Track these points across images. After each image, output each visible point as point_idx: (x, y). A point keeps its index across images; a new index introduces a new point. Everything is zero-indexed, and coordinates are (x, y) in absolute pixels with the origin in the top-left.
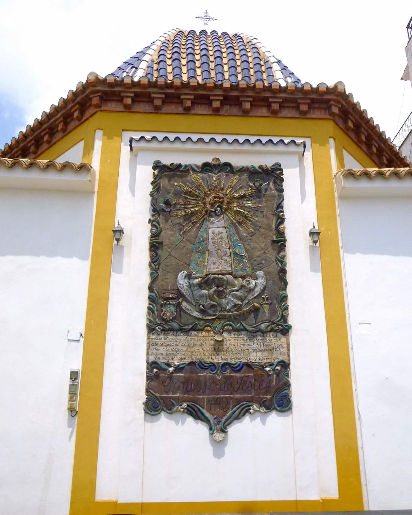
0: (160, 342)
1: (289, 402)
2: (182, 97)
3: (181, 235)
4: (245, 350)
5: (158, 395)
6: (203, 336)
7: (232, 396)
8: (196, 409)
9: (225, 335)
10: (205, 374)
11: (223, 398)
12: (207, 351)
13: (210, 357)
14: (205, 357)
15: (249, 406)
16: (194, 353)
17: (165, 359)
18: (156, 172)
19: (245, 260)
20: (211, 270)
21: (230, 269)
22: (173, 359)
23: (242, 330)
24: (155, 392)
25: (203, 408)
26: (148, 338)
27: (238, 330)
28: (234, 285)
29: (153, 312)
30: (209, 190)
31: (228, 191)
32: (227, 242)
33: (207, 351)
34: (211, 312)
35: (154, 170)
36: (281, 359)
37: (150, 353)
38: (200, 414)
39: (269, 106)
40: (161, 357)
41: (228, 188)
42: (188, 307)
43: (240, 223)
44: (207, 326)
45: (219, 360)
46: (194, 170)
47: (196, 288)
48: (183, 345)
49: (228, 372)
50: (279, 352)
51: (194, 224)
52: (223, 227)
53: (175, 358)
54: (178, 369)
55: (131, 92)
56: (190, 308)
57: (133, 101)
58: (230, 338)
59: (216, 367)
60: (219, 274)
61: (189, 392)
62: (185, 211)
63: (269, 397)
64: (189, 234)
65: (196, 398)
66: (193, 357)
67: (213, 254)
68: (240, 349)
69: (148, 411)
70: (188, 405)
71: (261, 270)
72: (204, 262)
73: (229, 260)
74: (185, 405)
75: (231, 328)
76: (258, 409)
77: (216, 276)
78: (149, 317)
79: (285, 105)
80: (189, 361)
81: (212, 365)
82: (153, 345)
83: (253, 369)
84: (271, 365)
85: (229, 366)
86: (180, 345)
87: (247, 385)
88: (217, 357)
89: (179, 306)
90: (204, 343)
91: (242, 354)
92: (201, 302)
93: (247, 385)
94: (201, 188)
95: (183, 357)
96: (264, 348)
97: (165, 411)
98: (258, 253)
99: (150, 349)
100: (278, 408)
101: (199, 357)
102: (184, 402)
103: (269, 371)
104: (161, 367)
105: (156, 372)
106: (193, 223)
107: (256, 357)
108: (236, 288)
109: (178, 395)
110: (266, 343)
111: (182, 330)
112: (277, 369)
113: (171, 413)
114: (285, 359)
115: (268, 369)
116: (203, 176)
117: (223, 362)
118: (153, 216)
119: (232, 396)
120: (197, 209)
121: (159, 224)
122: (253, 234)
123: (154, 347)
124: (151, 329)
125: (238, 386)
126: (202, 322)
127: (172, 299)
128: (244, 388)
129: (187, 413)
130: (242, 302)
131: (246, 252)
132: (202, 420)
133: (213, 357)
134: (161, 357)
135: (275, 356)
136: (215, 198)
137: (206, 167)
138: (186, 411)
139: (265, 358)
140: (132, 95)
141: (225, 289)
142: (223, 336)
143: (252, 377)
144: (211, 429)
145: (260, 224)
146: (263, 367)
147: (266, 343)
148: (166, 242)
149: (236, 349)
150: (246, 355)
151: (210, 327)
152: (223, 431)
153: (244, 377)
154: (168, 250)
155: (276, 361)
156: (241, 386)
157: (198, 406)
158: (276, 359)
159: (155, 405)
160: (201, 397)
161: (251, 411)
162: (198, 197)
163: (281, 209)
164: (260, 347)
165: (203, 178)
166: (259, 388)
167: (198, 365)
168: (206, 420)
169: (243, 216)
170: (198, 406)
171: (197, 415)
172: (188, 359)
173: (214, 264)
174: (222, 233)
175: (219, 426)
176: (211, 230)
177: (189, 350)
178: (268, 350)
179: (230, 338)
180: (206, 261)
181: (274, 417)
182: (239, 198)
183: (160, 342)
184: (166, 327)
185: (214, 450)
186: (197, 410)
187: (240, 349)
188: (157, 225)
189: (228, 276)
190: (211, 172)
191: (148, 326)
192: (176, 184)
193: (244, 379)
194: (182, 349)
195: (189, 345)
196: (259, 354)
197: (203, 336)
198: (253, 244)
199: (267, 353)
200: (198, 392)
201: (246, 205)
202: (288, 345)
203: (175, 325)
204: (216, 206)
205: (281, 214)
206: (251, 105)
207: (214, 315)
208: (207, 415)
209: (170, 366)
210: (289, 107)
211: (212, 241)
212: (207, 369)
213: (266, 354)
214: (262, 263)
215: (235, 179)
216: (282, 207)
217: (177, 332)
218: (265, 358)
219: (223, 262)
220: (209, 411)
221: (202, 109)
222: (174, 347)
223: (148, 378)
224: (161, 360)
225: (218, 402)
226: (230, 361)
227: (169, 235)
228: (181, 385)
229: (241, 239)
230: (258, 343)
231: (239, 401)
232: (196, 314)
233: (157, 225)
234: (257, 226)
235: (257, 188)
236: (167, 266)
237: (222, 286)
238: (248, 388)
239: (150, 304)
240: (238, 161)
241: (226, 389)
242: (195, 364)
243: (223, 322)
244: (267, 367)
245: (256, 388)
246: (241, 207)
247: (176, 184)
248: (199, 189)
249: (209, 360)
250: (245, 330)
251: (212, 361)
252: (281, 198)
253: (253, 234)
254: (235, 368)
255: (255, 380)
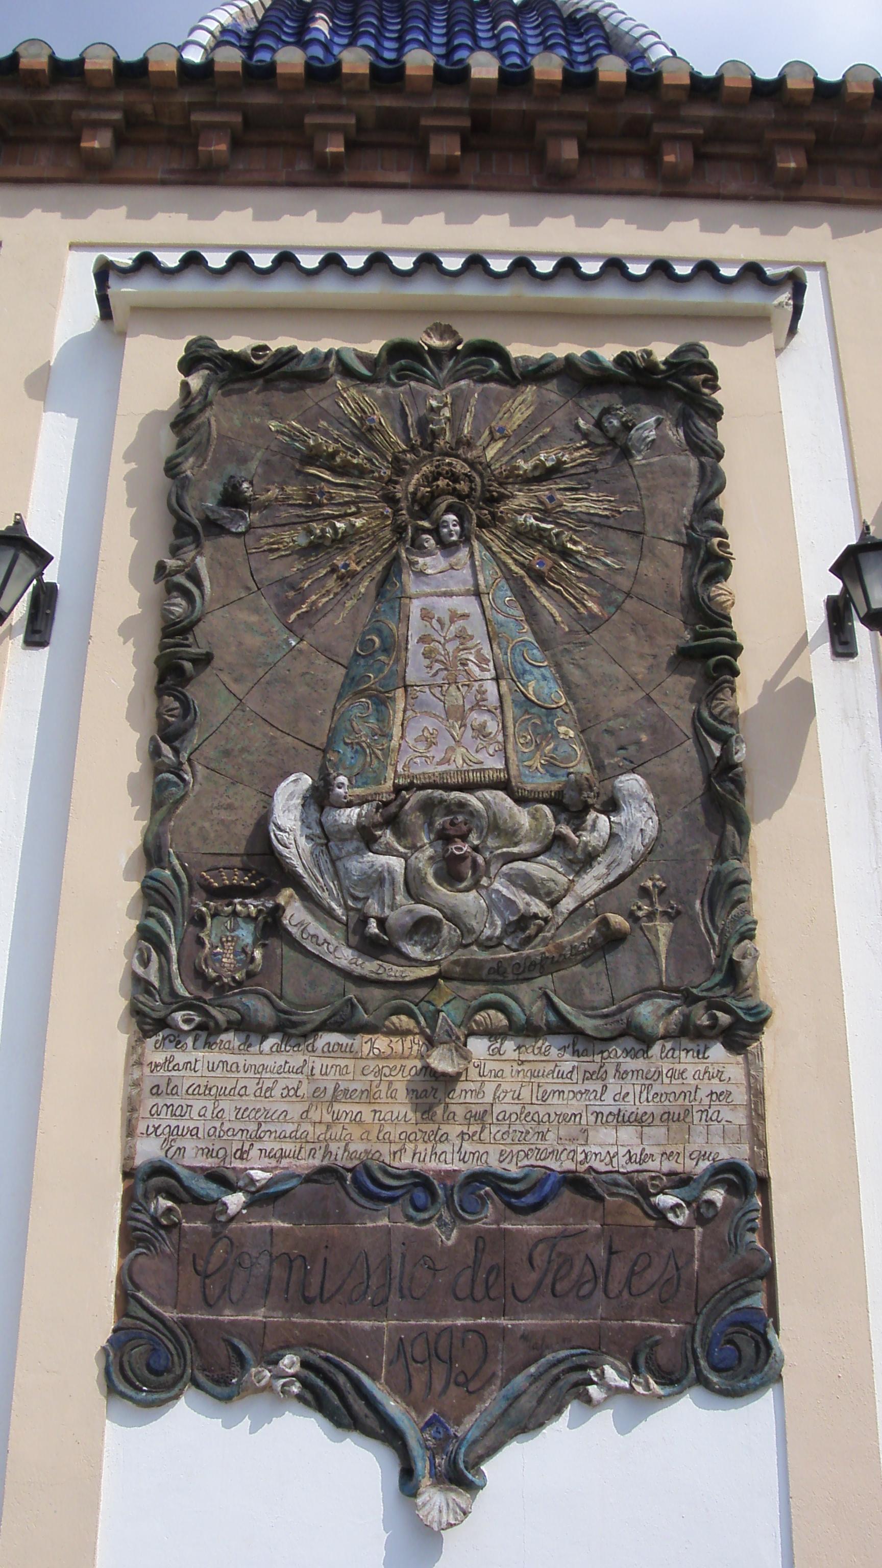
0: (186, 1079)
1: (764, 1349)
2: (309, 120)
3: (289, 628)
4: (564, 1118)
5: (170, 1314)
6: (379, 1057)
7: (503, 1322)
8: (341, 1379)
9: (478, 1046)
10: (385, 1222)
11: (467, 1329)
12: (394, 1122)
13: (410, 1147)
14: (385, 1149)
15: (583, 1368)
16: (337, 1130)
17: (209, 1153)
18: (196, 382)
19: (562, 729)
20: (414, 771)
21: (501, 766)
22: (242, 1155)
23: (552, 1031)
24: (160, 1303)
25: (374, 1377)
26: (135, 1060)
27: (527, 1030)
28: (511, 835)
29: (162, 949)
30: (413, 449)
31: (490, 453)
32: (486, 652)
33: (394, 1122)
34: (415, 951)
35: (187, 375)
36: (725, 1154)
37: (141, 1127)
38: (359, 1406)
39: (652, 158)
40: (190, 1145)
41: (493, 439)
42: (315, 927)
43: (540, 578)
44: (397, 1011)
45: (448, 1155)
46: (347, 371)
47: (351, 846)
48: (291, 1093)
49: (488, 1218)
50: (715, 1127)
51: (347, 578)
52: (467, 593)
53: (254, 1153)
54: (263, 1198)
55: (112, 108)
56: (323, 933)
57: (120, 141)
58: (496, 1066)
59: (433, 1194)
60: (449, 788)
61: (308, 1301)
62: (310, 532)
63: (673, 1327)
64: (323, 622)
65: (343, 1330)
66: (333, 1147)
67: (422, 704)
68: (542, 1111)
69: (123, 1387)
70: (305, 1364)
71: (633, 771)
72: (389, 736)
73: (493, 727)
74: (290, 1362)
75: (500, 1019)
76: (626, 1384)
77: (438, 793)
78: (140, 970)
79: (715, 149)
80: (317, 1162)
81: (421, 1181)
82: (156, 1091)
83: (600, 1199)
84: (680, 1181)
85: (498, 1190)
86: (277, 1092)
87: (574, 1275)
88: (440, 1148)
89: (271, 926)
90: (384, 1087)
91: (551, 1136)
92: (373, 907)
93: (574, 1275)
94: (378, 439)
95: (288, 1147)
96: (650, 1108)
97: (198, 1385)
98: (620, 702)
99: (144, 1112)
100: (714, 1378)
101: (358, 1147)
102: (288, 1347)
103: (674, 1208)
104: (187, 1189)
105: (164, 1208)
106: (341, 578)
107: (611, 1149)
108: (525, 848)
109: (259, 1315)
110: (657, 1088)
111: (291, 1029)
112: (711, 1203)
113: (228, 1399)
114: (741, 1153)
115: (666, 1200)
116: (386, 396)
117: (465, 1168)
118: (175, 551)
119: (503, 1322)
120: (358, 522)
121: (199, 584)
122: (594, 623)
123: (160, 1101)
124: (149, 1019)
125: (534, 1276)
126: (377, 993)
127: (245, 892)
128: (558, 1287)
129: (300, 1397)
130: (553, 905)
131: (569, 694)
132: (368, 1433)
133: (421, 1147)
134: (190, 1145)
135: (698, 1143)
136: (436, 476)
137: (403, 358)
138: (296, 1389)
139: (656, 1151)
140: (117, 116)
141: (476, 849)
142: (466, 1057)
143: (598, 1236)
144: (407, 1474)
145: (624, 583)
146: (641, 1190)
147: (657, 1088)
148: (224, 656)
149: (523, 1115)
150: (572, 1140)
151: (411, 1015)
152: (460, 1478)
153: (565, 1235)
154: (234, 687)
155: (705, 1164)
156: (549, 1280)
157: (349, 1366)
158: (704, 1156)
159: (152, 1360)
160: (367, 1324)
161: (593, 1390)
162: (362, 472)
163: (713, 524)
164: (629, 1106)
165: (385, 403)
166: (628, 1284)
167: (355, 1180)
168: (388, 1434)
169: (552, 550)
170: (349, 1366)
171: (339, 1402)
172: (312, 1153)
173: (431, 744)
174: (465, 616)
175: (440, 1464)
176: (415, 608)
177: (315, 1115)
178: (668, 1118)
179: (496, 1066)
180: (396, 731)
181: (688, 1416)
182: (538, 480)
183: (186, 1079)
184: (214, 1012)
185: (163, 412)
186: (346, 1386)
187: (532, 1106)
188: (189, 585)
189: (488, 794)
190: (421, 378)
191: (136, 1011)
192: (273, 425)
193: (562, 1247)
194: (279, 1107)
195: (317, 1095)
196: (628, 1134)
197: (379, 1057)
198: (600, 665)
199: (663, 1130)
200: (351, 1302)
201: (568, 506)
202: (757, 1095)
203: (263, 1012)
204: (443, 506)
205: (716, 540)
206: (583, 151)
207: (431, 964)
208: (393, 1406)
209: (232, 1188)
210: (731, 158)
211: (422, 648)
212: (391, 1200)
213: (658, 1132)
214: (638, 743)
215: (522, 405)
216: (718, 516)
217: (264, 1038)
218: (656, 1151)
219: (469, 733)
220: (404, 1391)
221: (376, 216)
222: (250, 1102)
223: (132, 1238)
224: (192, 1156)
225: (439, 1350)
226: (494, 1164)
227: (236, 626)
228: (278, 1272)
229: (544, 644)
230: (629, 1082)
231: (536, 1345)
232: (345, 957)
233: (189, 585)
234: (614, 588)
235: (612, 441)
236: (227, 753)
237: (464, 838)
238: (579, 1284)
239: (149, 915)
240: (522, 349)
241: (479, 1292)
242: (342, 1179)
243: (470, 990)
244: (662, 1191)
245: (615, 1287)
246: (545, 513)
247: (273, 425)
248: (371, 446)
249: (406, 1161)
250: (564, 1027)
251: (417, 1166)
252: (712, 481)
253: (594, 623)
254: (519, 1195)
255: (611, 1252)
